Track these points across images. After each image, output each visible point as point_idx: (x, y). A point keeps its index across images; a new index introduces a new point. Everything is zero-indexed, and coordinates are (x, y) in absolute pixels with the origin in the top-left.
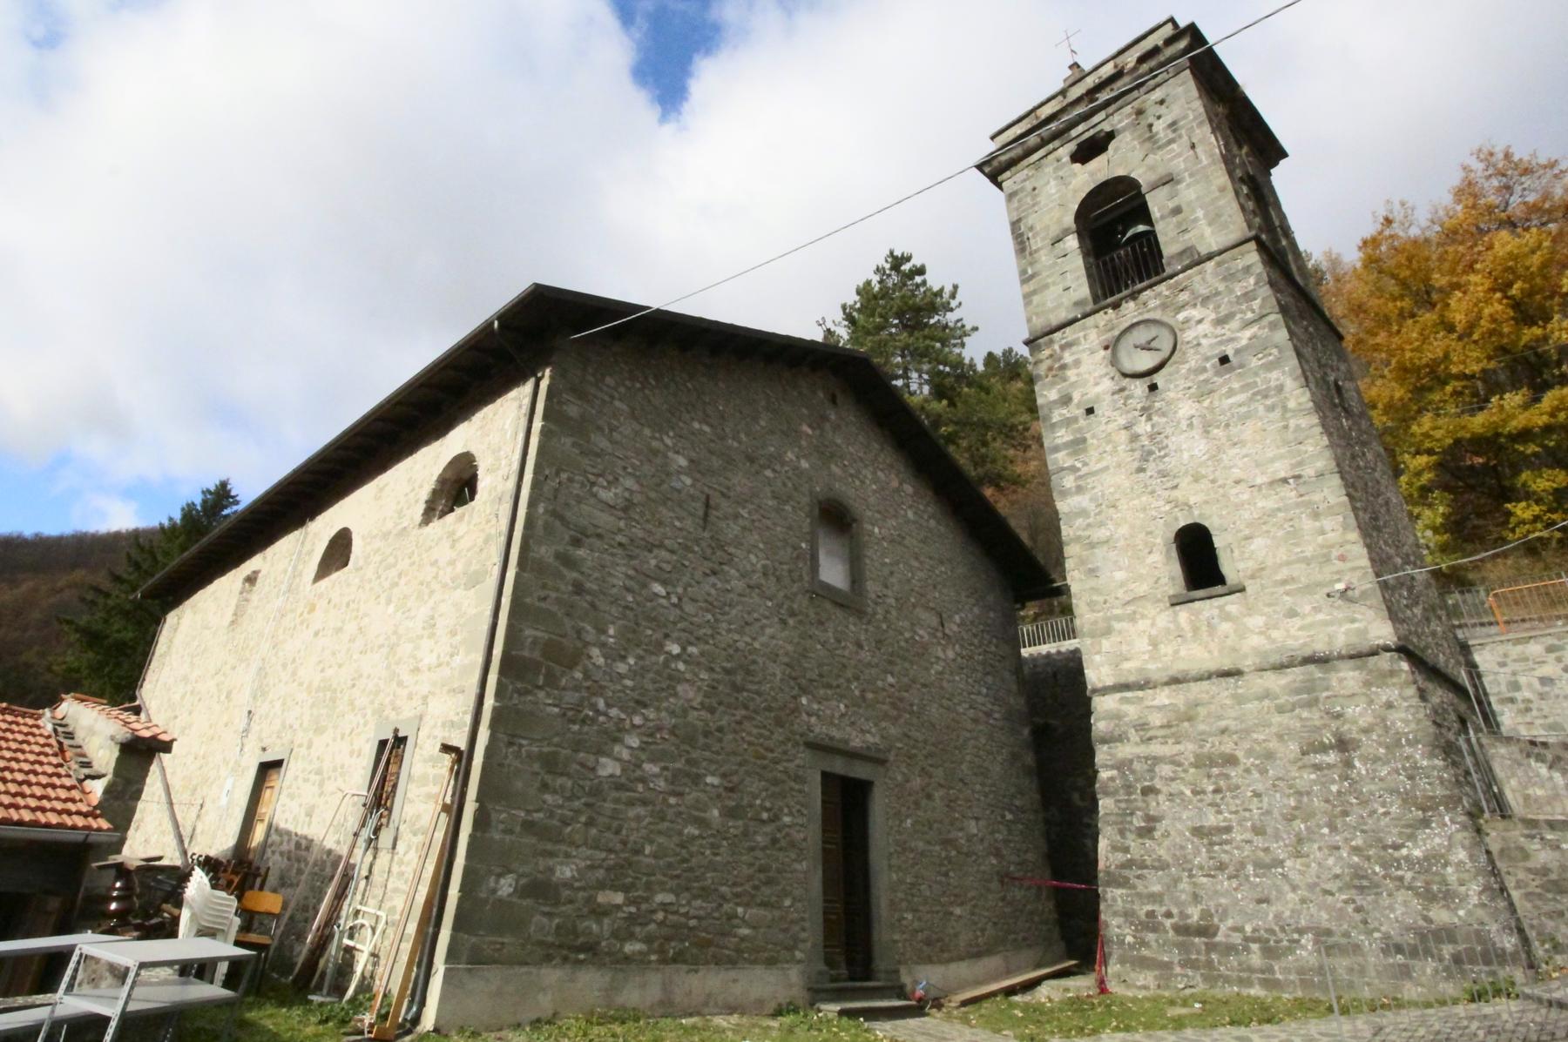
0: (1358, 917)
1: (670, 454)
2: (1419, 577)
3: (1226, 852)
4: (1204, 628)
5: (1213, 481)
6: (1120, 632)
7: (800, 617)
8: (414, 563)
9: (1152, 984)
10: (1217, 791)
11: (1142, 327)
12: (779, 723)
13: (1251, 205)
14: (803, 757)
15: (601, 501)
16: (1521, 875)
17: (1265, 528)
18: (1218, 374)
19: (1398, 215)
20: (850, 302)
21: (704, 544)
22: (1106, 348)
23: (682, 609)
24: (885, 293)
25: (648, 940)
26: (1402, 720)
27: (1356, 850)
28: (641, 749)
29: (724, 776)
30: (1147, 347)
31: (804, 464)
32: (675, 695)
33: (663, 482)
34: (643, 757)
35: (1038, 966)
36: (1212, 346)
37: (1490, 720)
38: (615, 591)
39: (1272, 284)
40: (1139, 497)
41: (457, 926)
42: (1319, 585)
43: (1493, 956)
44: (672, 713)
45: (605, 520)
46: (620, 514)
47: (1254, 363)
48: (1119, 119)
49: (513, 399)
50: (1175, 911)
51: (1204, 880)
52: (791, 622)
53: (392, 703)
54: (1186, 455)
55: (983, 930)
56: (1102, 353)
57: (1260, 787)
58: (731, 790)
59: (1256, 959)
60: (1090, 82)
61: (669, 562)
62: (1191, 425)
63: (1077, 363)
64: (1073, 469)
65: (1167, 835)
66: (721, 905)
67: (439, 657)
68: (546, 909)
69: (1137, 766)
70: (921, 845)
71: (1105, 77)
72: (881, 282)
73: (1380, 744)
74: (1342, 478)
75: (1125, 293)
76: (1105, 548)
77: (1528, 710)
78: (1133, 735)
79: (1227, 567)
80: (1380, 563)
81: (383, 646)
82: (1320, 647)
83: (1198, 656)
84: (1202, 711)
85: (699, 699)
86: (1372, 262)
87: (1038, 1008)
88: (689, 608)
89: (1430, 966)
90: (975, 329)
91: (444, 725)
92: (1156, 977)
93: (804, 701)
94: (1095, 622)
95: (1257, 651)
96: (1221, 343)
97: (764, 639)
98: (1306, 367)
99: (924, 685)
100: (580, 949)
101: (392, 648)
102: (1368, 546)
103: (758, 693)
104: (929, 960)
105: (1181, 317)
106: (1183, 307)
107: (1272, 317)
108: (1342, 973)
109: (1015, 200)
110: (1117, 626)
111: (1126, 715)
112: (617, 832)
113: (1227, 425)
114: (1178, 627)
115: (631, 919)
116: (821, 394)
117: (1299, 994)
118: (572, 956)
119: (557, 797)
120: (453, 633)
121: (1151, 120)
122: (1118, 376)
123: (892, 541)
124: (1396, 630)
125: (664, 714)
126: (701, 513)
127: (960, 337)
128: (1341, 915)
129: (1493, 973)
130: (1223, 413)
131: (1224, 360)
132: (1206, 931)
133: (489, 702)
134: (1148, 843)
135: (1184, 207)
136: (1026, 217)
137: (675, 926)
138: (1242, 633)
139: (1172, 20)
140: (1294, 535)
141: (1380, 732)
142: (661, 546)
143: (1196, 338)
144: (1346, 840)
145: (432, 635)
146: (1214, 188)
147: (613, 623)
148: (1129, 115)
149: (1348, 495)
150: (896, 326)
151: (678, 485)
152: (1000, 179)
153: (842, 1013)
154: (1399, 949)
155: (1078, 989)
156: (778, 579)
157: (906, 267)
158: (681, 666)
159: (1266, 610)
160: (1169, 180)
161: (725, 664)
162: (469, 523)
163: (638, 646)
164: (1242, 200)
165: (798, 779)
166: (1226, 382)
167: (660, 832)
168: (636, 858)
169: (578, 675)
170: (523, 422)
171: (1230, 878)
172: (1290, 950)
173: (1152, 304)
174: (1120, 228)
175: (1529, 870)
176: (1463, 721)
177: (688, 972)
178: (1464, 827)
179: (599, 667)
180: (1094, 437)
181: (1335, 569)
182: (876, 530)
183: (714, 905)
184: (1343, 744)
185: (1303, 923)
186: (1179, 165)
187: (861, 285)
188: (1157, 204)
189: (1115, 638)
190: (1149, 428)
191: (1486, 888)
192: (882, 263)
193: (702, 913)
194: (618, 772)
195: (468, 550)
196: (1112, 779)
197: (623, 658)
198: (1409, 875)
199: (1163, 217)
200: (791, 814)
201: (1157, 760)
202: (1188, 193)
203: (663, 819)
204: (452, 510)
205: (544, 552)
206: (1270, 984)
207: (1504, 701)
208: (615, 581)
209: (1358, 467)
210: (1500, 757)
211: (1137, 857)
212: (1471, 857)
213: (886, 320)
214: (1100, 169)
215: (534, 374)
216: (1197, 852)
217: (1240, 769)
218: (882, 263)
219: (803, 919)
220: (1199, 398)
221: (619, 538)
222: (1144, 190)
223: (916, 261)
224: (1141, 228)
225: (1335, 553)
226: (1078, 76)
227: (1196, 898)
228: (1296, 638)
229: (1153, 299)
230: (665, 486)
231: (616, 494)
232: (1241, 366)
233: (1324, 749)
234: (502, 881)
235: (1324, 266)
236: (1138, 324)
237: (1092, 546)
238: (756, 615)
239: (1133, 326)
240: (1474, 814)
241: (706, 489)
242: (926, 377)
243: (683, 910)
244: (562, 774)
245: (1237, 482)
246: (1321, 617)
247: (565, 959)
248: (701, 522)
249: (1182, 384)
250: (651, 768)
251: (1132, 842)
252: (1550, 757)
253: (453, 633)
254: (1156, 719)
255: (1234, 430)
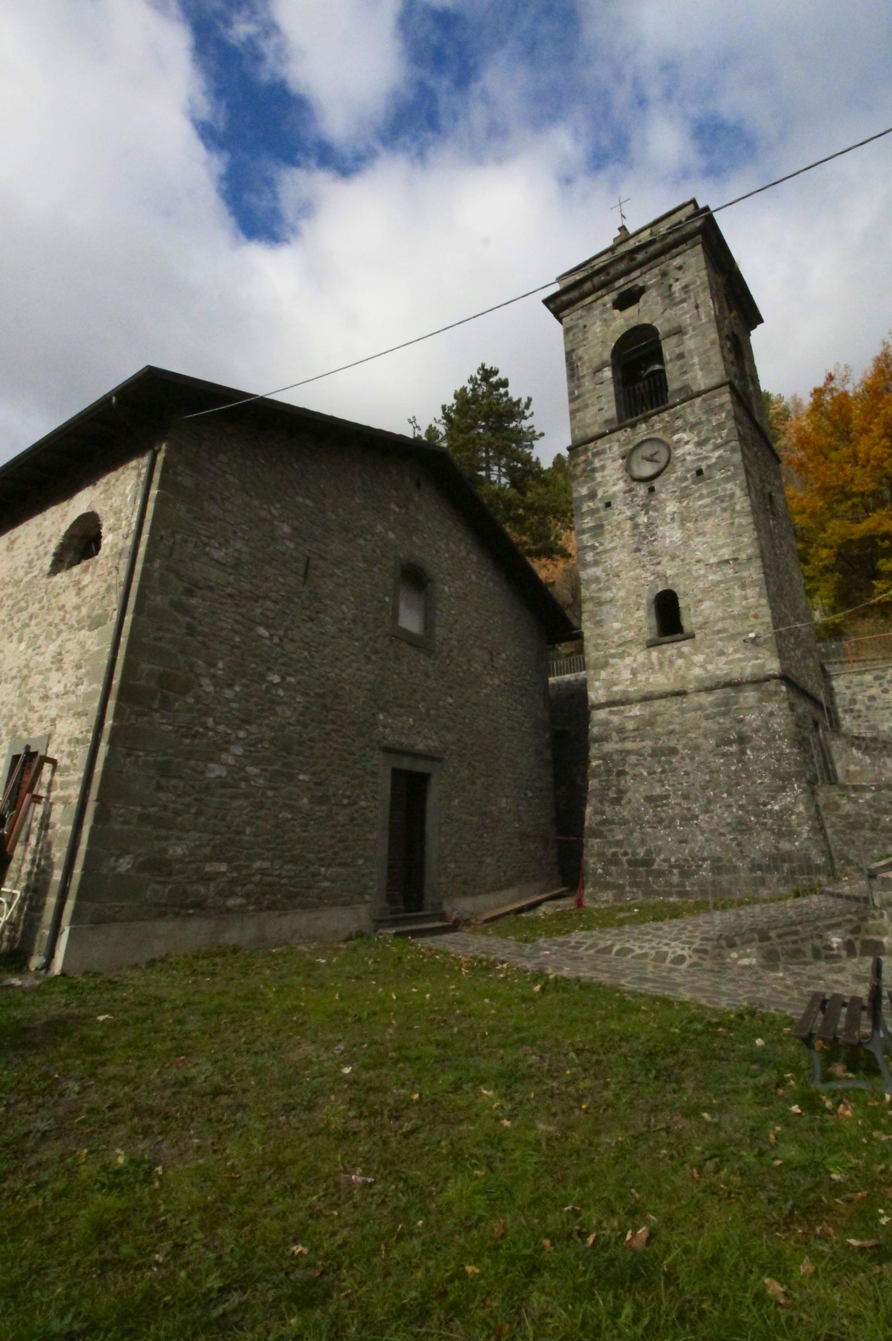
0: (738, 849)
1: (276, 522)
2: (803, 630)
3: (664, 811)
4: (667, 663)
5: (683, 560)
6: (613, 666)
7: (382, 655)
8: (43, 607)
9: (611, 899)
10: (663, 772)
11: (648, 443)
12: (360, 734)
13: (731, 357)
14: (379, 758)
15: (212, 559)
16: (834, 819)
17: (711, 594)
18: (694, 483)
19: (838, 377)
20: (449, 404)
21: (303, 597)
22: (623, 458)
23: (282, 648)
24: (475, 398)
25: (247, 896)
26: (778, 724)
27: (741, 807)
28: (245, 756)
29: (314, 774)
30: (651, 459)
31: (391, 535)
32: (275, 714)
33: (269, 545)
34: (246, 762)
35: (541, 893)
36: (693, 461)
37: (835, 723)
38: (223, 633)
39: (736, 418)
40: (634, 570)
41: (80, 897)
42: (740, 634)
43: (810, 868)
44: (272, 728)
45: (215, 575)
46: (230, 570)
47: (718, 476)
48: (650, 278)
49: (134, 468)
50: (630, 851)
51: (650, 830)
52: (374, 657)
53: (24, 725)
54: (668, 541)
55: (505, 872)
56: (620, 461)
57: (689, 768)
58: (319, 784)
59: (675, 879)
60: (632, 243)
61: (272, 611)
62: (673, 519)
63: (603, 468)
64: (593, 548)
65: (629, 802)
66: (307, 867)
67: (65, 686)
68: (162, 879)
69: (616, 757)
70: (465, 817)
71: (643, 242)
72: (473, 390)
73: (763, 739)
74: (763, 561)
75: (640, 416)
76: (609, 606)
77: (859, 716)
78: (615, 736)
79: (689, 621)
80: (778, 620)
81: (14, 678)
82: (736, 676)
83: (660, 681)
84: (660, 719)
85: (294, 718)
86: (817, 406)
87: (537, 920)
88: (289, 647)
89: (776, 875)
90: (542, 435)
91: (70, 742)
92: (614, 895)
93: (381, 716)
94: (597, 659)
95: (698, 679)
96: (698, 460)
97: (350, 671)
98: (751, 481)
99: (475, 704)
100: (188, 907)
101: (25, 679)
102: (773, 609)
103: (344, 712)
104: (465, 894)
105: (675, 438)
106: (676, 431)
107: (734, 443)
108: (725, 885)
109: (571, 334)
110: (611, 661)
111: (612, 722)
112: (223, 819)
113: (696, 520)
114: (652, 663)
115: (232, 881)
116: (408, 479)
117: (699, 899)
118: (183, 912)
119: (169, 795)
120: (78, 667)
121: (671, 281)
122: (629, 480)
123: (458, 598)
124: (782, 664)
125: (264, 729)
126: (302, 571)
127: (531, 441)
128: (728, 848)
129: (810, 880)
130: (694, 511)
131: (700, 472)
132: (647, 862)
133: (109, 723)
134: (617, 808)
135: (686, 354)
136: (578, 348)
137: (270, 885)
138: (690, 665)
139: (694, 202)
140: (729, 599)
141: (764, 731)
142: (266, 597)
143: (683, 455)
144: (736, 801)
145: (59, 669)
146: (707, 341)
147: (222, 658)
148: (656, 276)
149: (765, 573)
150: (483, 427)
151: (282, 548)
152: (561, 315)
153: (396, 935)
154: (760, 868)
155: (565, 906)
156: (365, 626)
157: (494, 379)
158: (281, 692)
159: (706, 650)
160: (679, 331)
161: (317, 690)
162: (93, 573)
163: (244, 677)
164: (725, 353)
165: (373, 774)
166: (699, 489)
167: (258, 818)
168: (238, 838)
169: (191, 700)
170: (141, 489)
171: (665, 828)
172: (697, 872)
173: (658, 426)
174: (644, 365)
175: (838, 817)
176: (816, 724)
177: (279, 916)
178: (805, 791)
179: (207, 693)
180: (609, 524)
181: (750, 623)
182: (446, 589)
183: (302, 867)
184: (742, 740)
185: (705, 854)
186: (687, 320)
187: (458, 390)
188: (669, 349)
189: (610, 670)
190: (646, 520)
191: (812, 829)
192: (474, 373)
193: (292, 874)
194: (224, 774)
195: (92, 597)
196: (598, 766)
197: (231, 686)
198: (770, 822)
199: (671, 360)
200: (366, 799)
201: (628, 752)
202: (690, 343)
203: (261, 808)
204: (79, 563)
205: (158, 600)
206: (682, 894)
207: (846, 711)
208: (224, 625)
209: (776, 554)
210: (836, 746)
211: (610, 817)
212: (807, 809)
213: (476, 423)
214: (632, 317)
215: (151, 447)
216: (646, 813)
217: (678, 758)
218: (474, 373)
219: (372, 873)
220: (680, 500)
221: (229, 590)
222: (660, 337)
223: (501, 375)
224: (657, 367)
225: (752, 612)
226: (624, 237)
227: (643, 842)
228: (721, 669)
229: (659, 421)
230: (271, 548)
231: (226, 554)
232: (710, 478)
233: (730, 743)
234: (122, 861)
235: (791, 407)
236: (646, 440)
237: (600, 604)
238: (345, 653)
239: (643, 443)
240: (812, 783)
241: (307, 553)
242: (504, 470)
243: (277, 873)
244: (174, 777)
245: (698, 561)
246: (738, 656)
247: (177, 914)
248: (302, 579)
249: (671, 488)
250: (252, 770)
251: (607, 808)
252: (864, 746)
253: (78, 667)
254: (630, 725)
255: (700, 524)
